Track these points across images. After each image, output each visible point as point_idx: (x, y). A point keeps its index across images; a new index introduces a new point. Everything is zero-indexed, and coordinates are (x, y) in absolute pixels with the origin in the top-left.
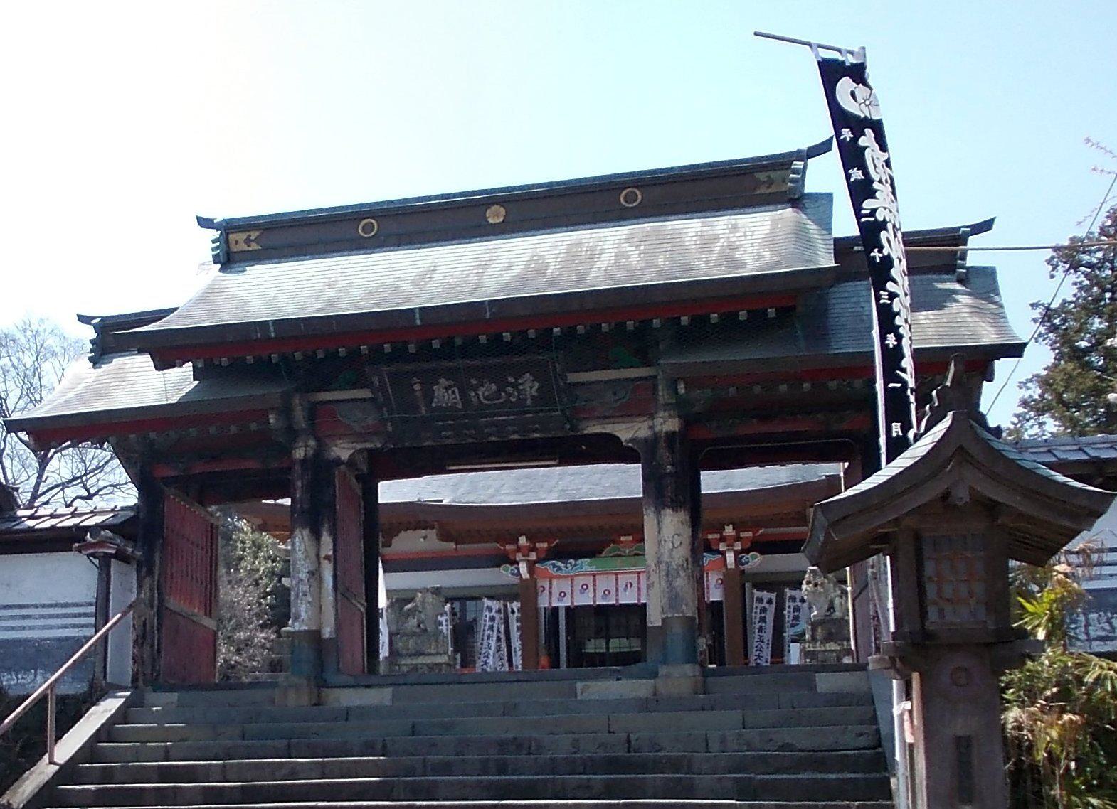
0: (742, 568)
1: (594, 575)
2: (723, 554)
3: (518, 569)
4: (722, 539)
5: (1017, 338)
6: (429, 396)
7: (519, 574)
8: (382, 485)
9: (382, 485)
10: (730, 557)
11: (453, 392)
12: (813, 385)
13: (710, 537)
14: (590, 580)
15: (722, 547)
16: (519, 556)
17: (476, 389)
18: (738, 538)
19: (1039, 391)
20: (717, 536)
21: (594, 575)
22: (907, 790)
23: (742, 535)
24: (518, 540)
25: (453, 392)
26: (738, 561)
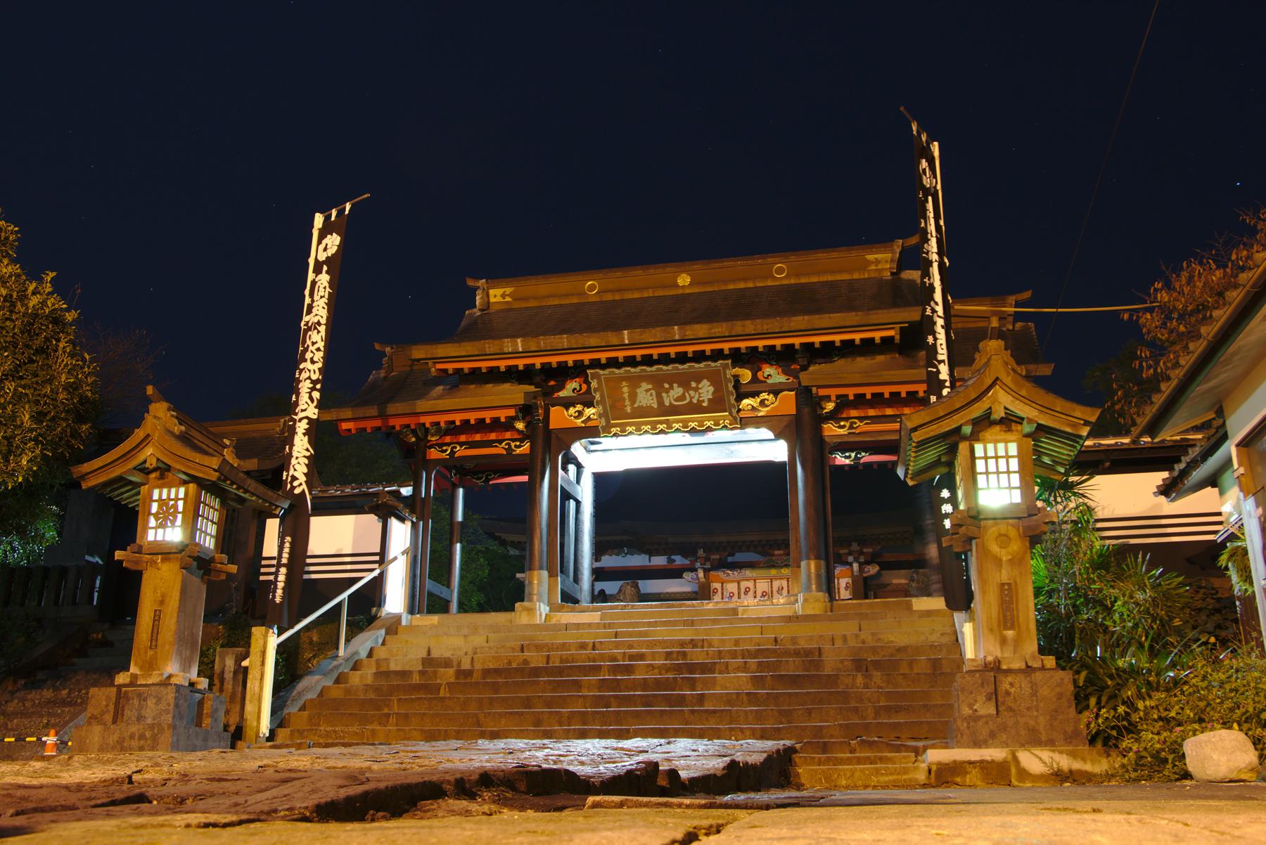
0: (864, 575)
1: (755, 580)
2: (851, 564)
3: (697, 575)
4: (850, 554)
5: (1229, 417)
6: (633, 397)
7: (698, 578)
8: (527, 480)
9: (527, 480)
10: (856, 566)
11: (651, 395)
12: (148, 383)
13: (841, 552)
14: (784, 583)
15: (850, 559)
16: (850, 559)
17: (667, 391)
18: (861, 553)
19: (152, 407)
20: (846, 551)
21: (755, 580)
22: (666, 805)
23: (865, 550)
24: (851, 545)
25: (651, 395)
26: (861, 570)
